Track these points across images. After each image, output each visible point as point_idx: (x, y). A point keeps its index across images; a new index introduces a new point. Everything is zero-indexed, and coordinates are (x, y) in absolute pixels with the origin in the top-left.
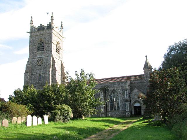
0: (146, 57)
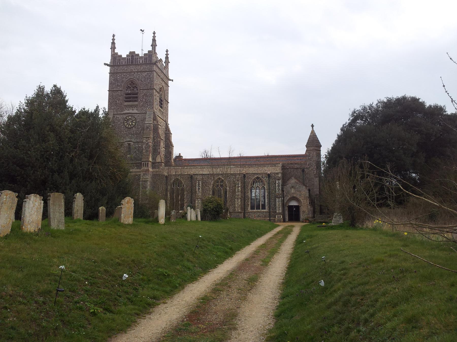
0: (312, 126)
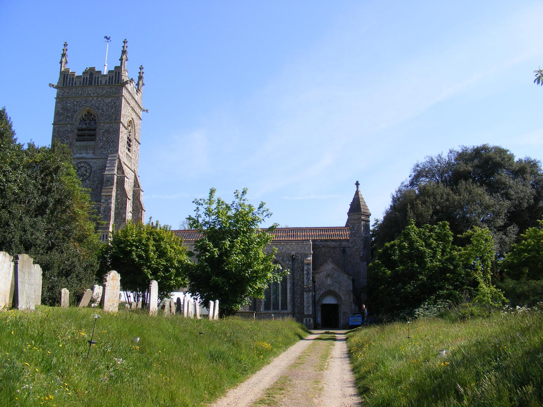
0: (357, 184)
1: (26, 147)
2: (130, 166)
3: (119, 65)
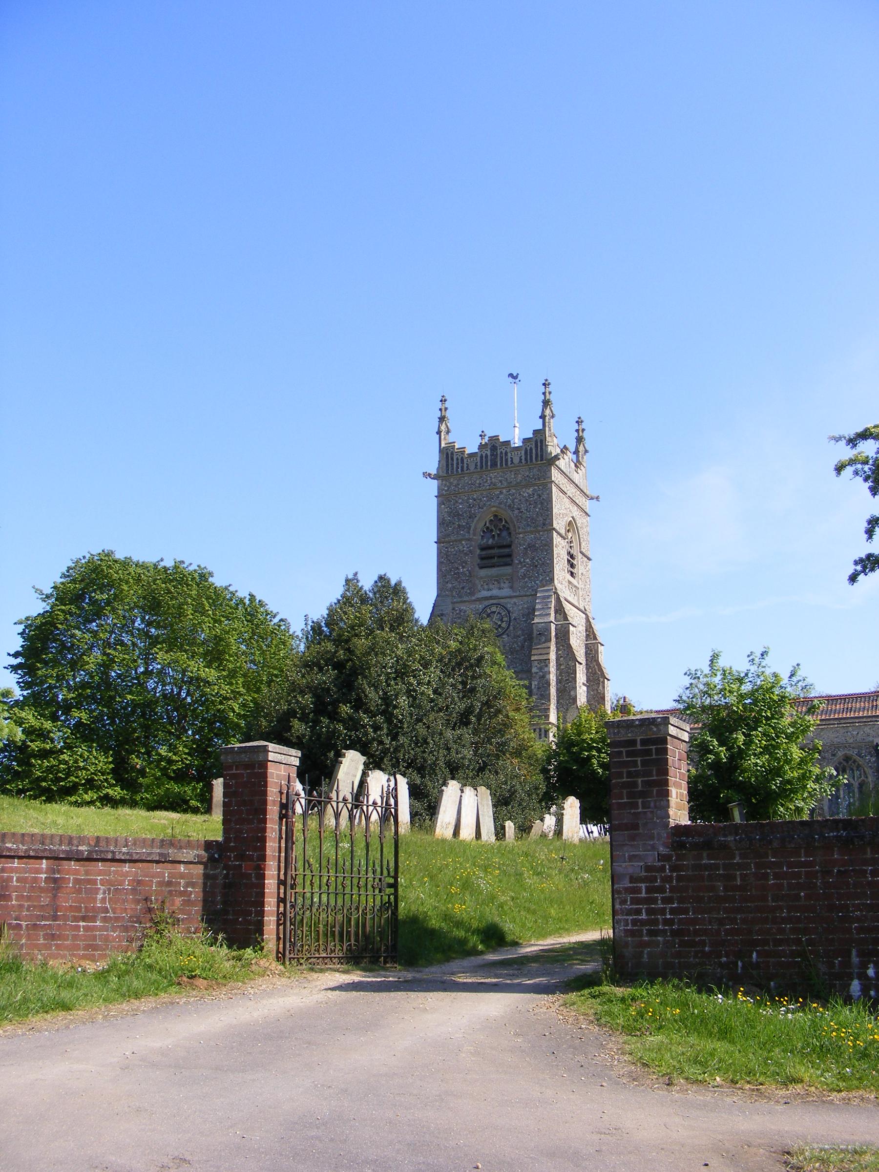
1: (393, 583)
2: (576, 604)
3: (541, 427)
